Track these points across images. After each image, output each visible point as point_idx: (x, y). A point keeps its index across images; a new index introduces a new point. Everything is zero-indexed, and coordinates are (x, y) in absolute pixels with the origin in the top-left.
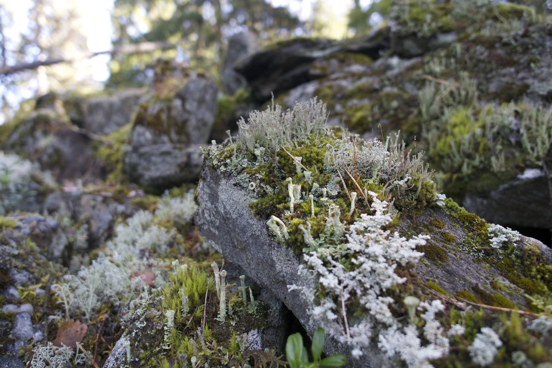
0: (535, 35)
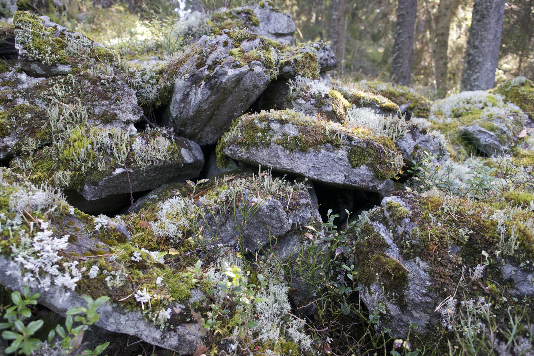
0: (119, 82)
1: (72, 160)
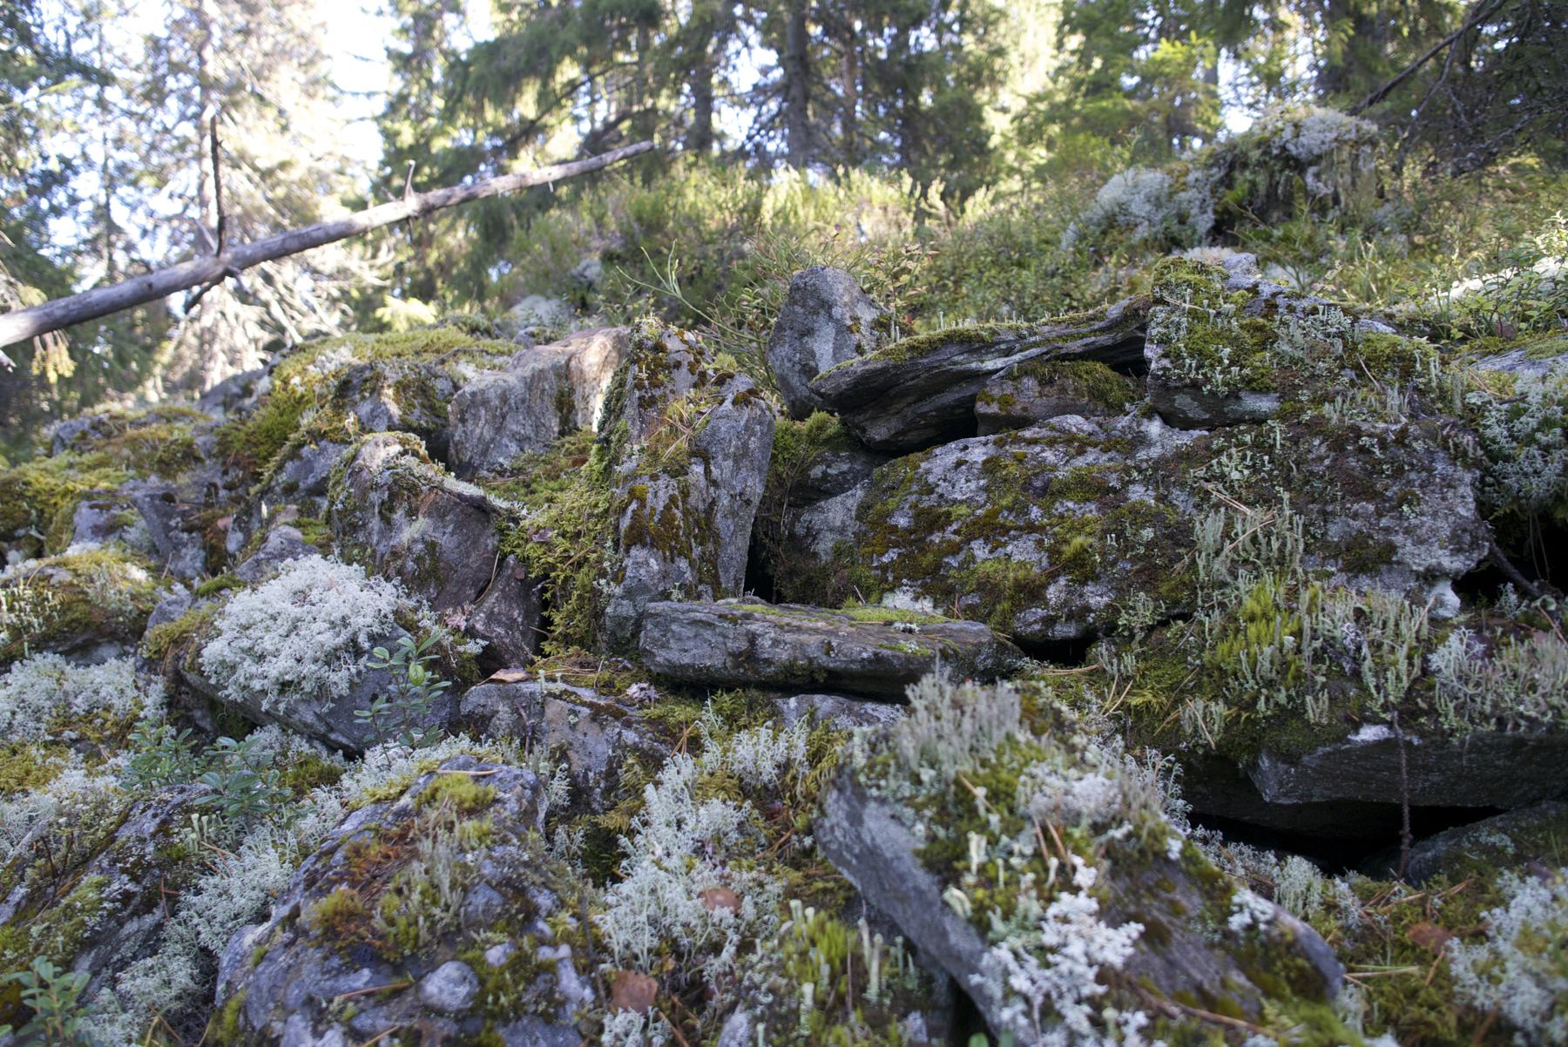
0: (1418, 446)
1: (1235, 674)
